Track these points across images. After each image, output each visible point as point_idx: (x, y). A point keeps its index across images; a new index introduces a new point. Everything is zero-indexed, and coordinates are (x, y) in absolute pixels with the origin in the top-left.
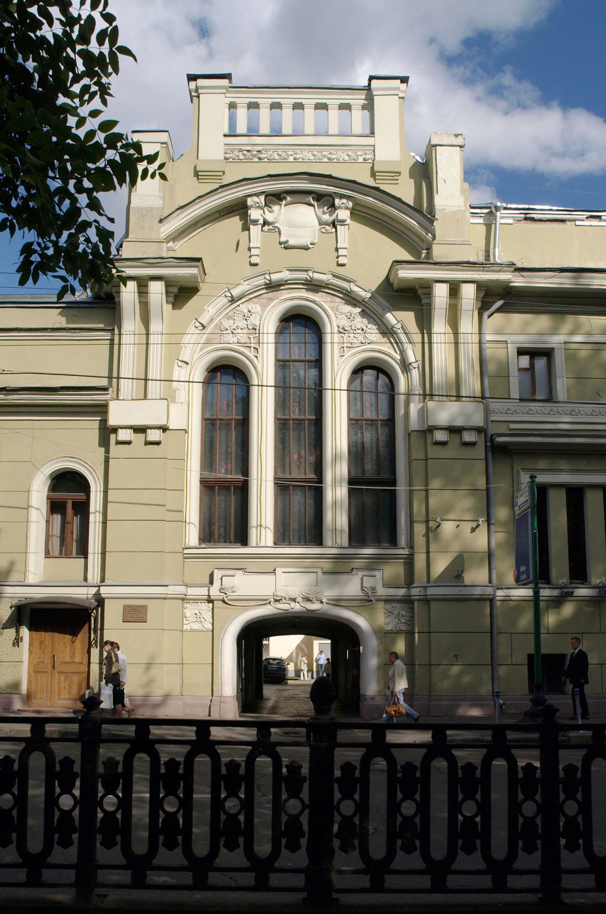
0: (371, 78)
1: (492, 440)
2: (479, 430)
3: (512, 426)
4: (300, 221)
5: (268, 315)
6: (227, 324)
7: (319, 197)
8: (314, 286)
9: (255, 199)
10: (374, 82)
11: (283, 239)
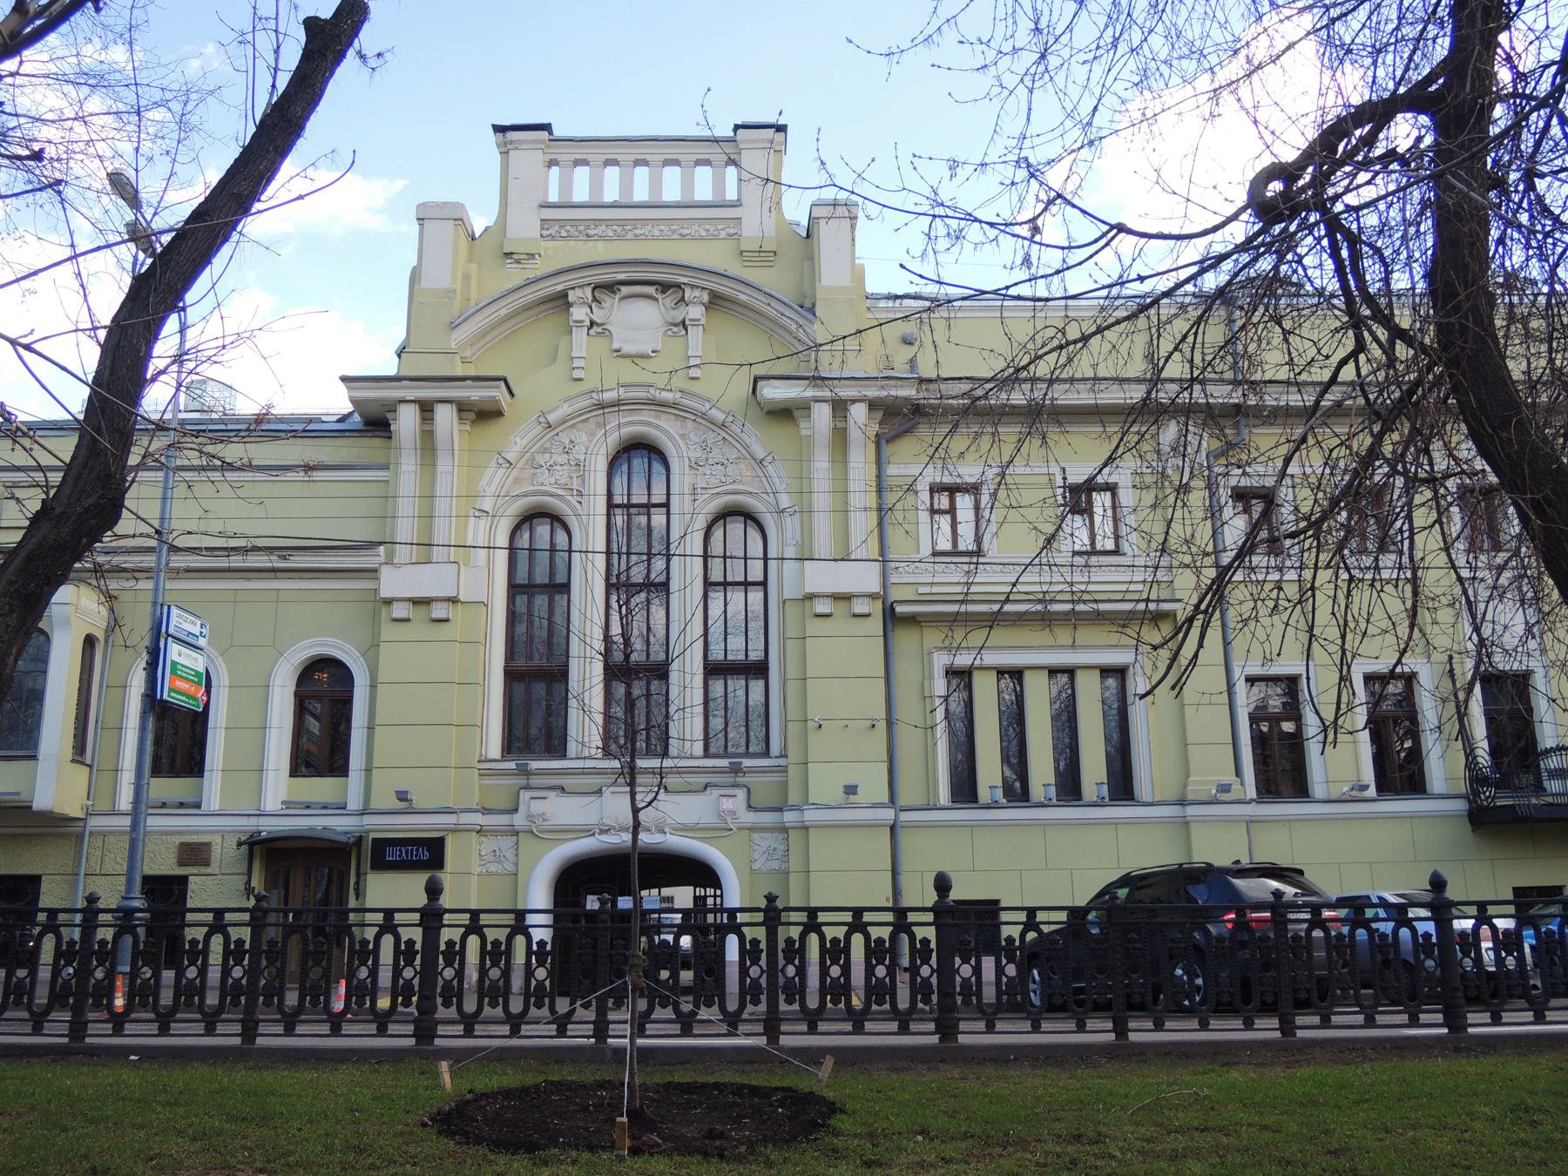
0: (737, 127)
1: (893, 610)
4: (638, 322)
6: (541, 459)
7: (665, 287)
9: (579, 292)
10: (740, 131)
11: (616, 346)
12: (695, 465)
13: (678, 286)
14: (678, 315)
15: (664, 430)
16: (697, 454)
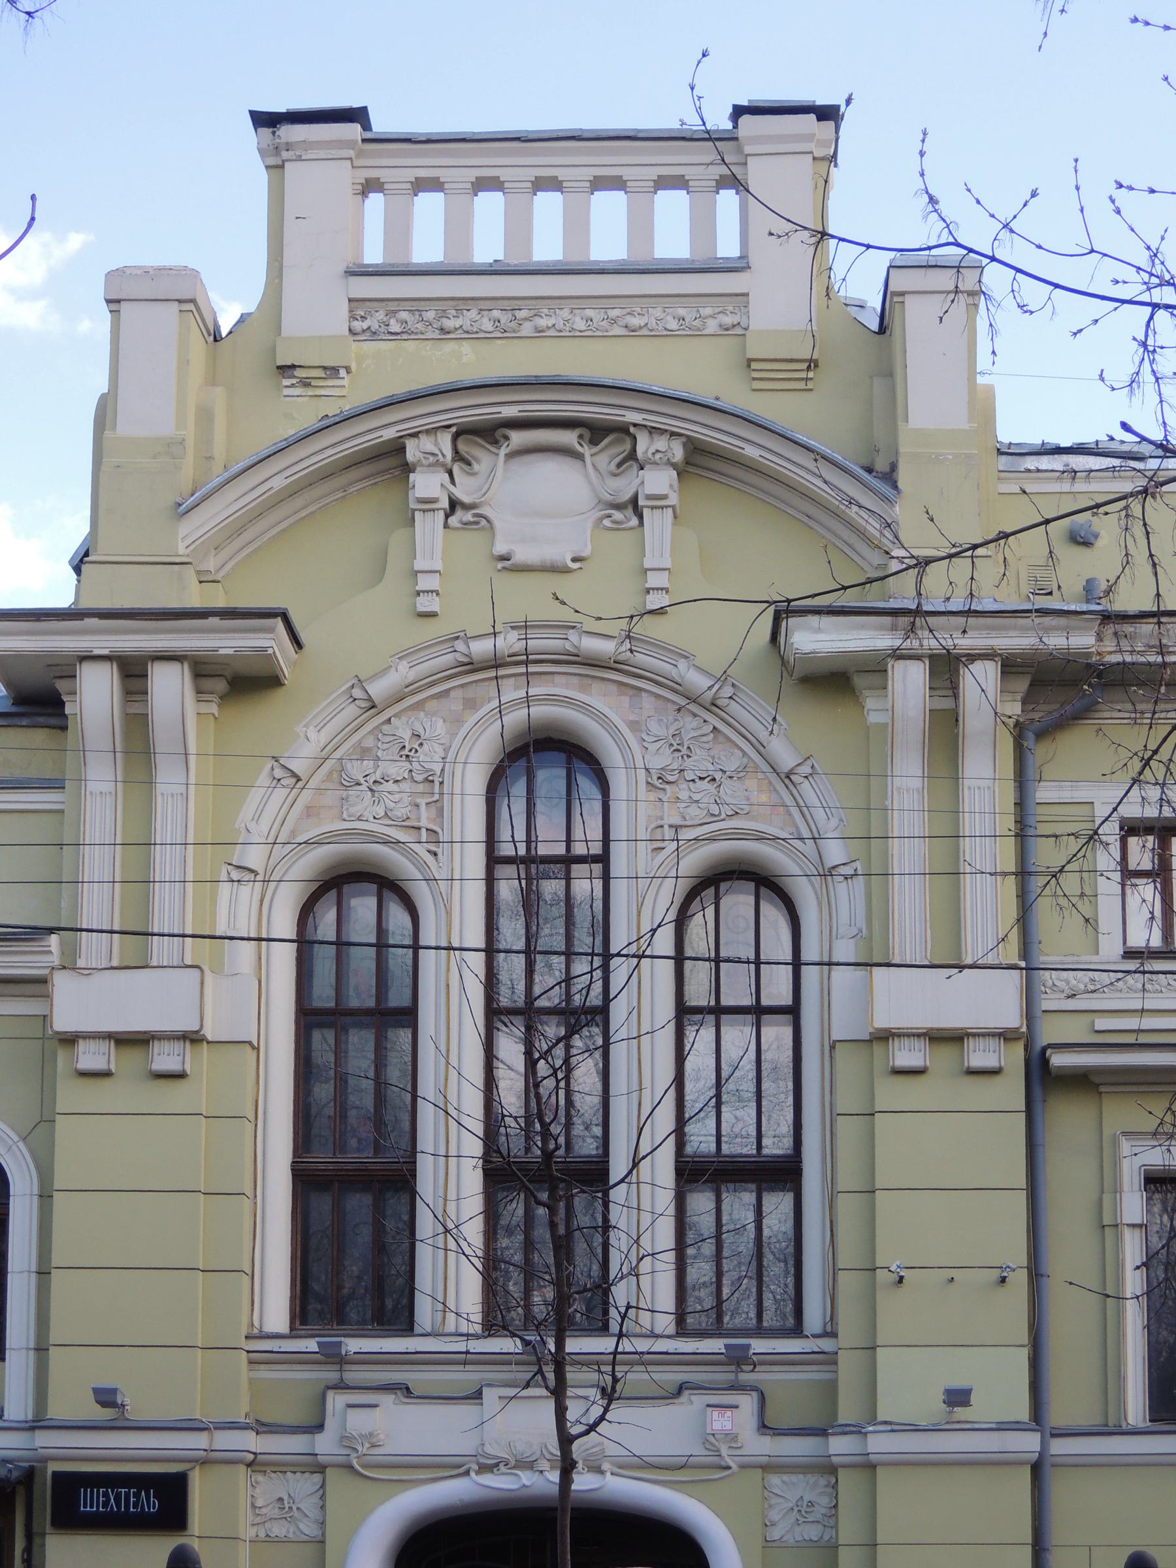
2: (1006, 1036)
3: (1102, 1023)
5: (467, 750)
7: (596, 432)
9: (427, 443)
11: (500, 548)
12: (660, 781)
13: (623, 430)
14: (624, 487)
15: (598, 713)
16: (662, 759)
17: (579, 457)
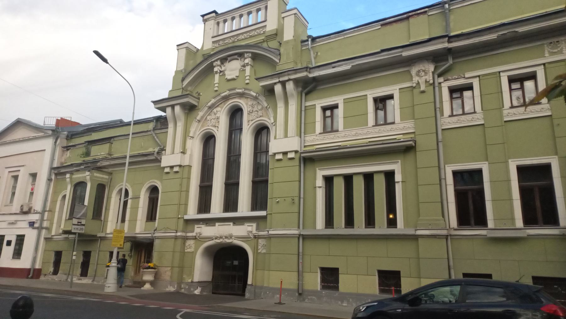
8: (241, 95)
9: (216, 63)
15: (243, 103)
17: (238, 59)
